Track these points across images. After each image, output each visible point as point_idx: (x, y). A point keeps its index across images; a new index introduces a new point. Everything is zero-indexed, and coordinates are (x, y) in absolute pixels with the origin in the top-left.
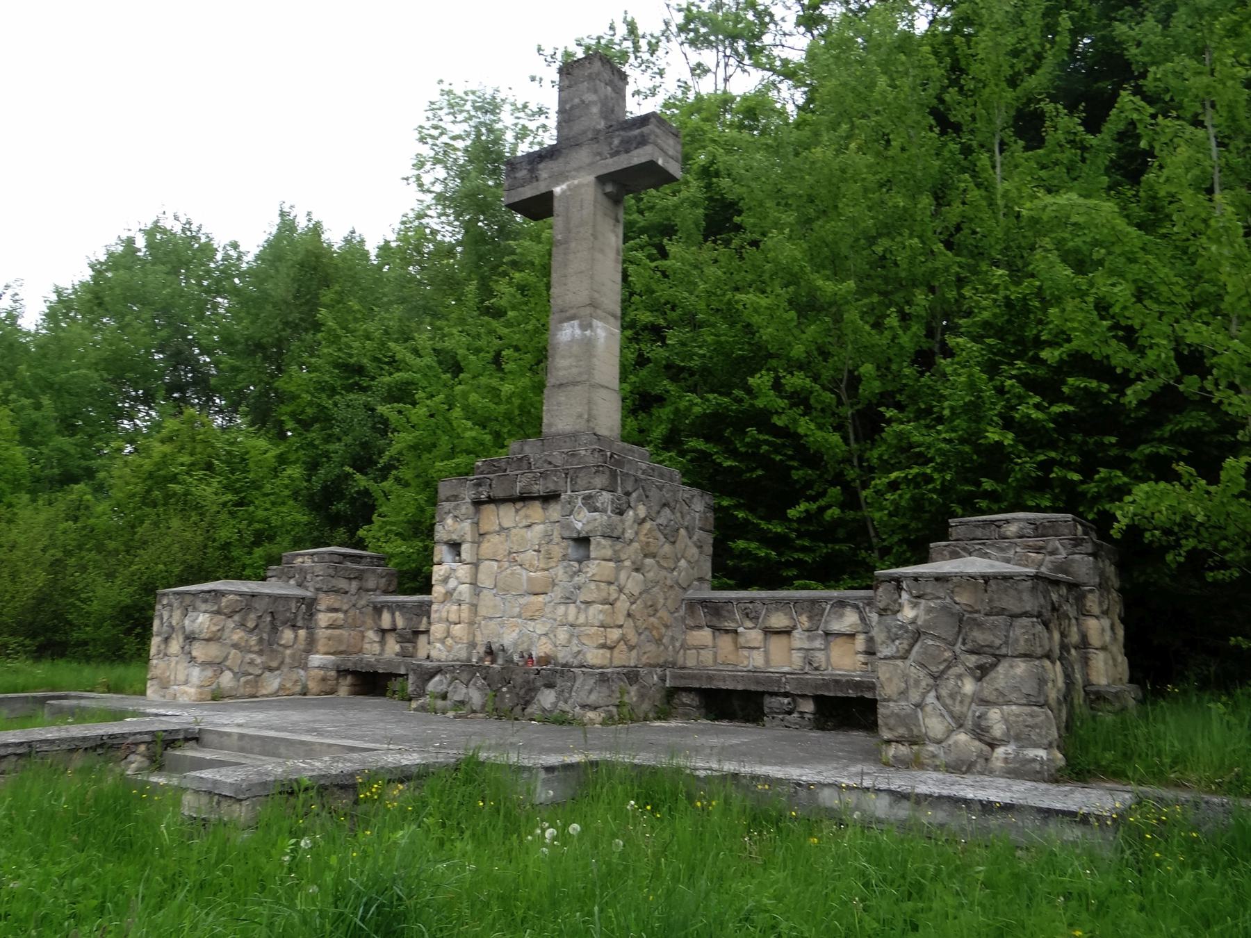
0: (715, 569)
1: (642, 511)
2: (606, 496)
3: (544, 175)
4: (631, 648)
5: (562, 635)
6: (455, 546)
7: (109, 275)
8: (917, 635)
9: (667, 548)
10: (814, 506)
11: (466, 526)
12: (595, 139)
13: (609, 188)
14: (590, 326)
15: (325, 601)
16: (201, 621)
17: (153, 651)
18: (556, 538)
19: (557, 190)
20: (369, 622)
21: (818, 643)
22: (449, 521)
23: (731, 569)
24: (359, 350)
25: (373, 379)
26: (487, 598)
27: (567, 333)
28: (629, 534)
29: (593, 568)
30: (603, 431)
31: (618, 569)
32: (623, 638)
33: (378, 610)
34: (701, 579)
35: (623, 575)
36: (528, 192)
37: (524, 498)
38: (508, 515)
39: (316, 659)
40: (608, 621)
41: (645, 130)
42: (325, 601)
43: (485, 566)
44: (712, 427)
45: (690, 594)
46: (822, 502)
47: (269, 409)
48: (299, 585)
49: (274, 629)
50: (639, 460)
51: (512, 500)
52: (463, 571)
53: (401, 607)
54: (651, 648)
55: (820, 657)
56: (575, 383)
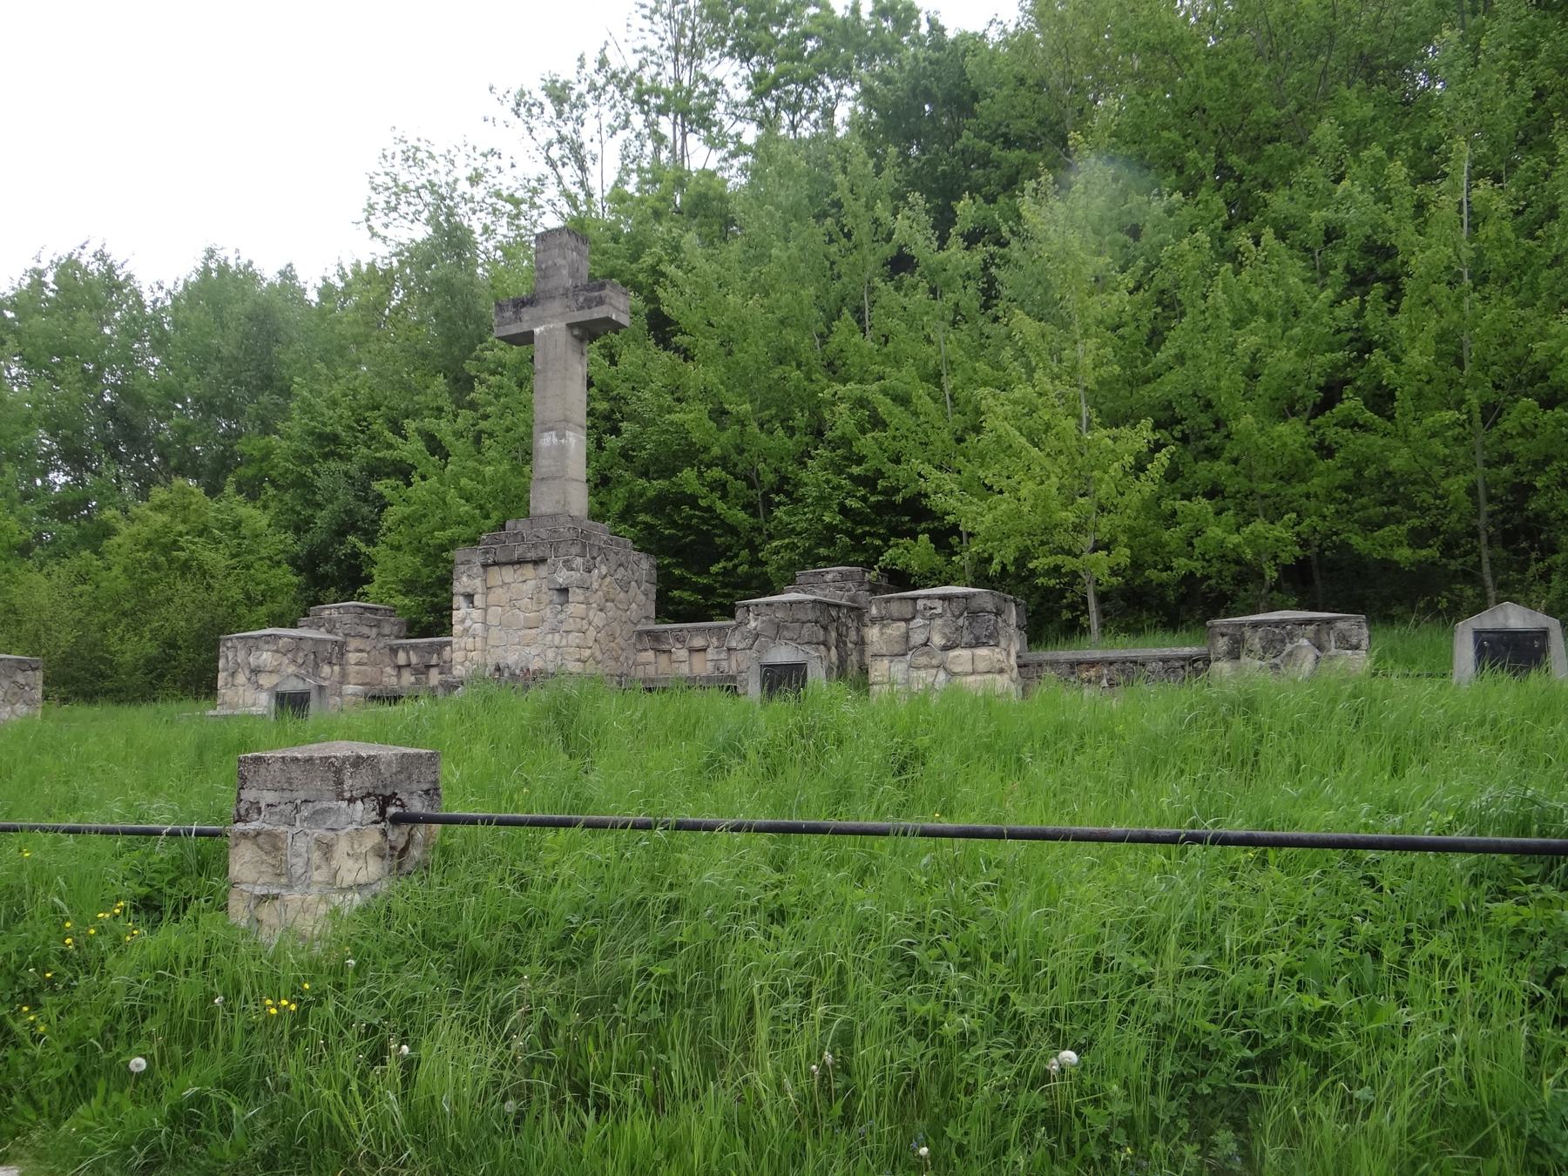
0: (658, 612)
1: (604, 570)
2: (579, 560)
3: (526, 317)
4: (598, 663)
5: (550, 654)
6: (469, 597)
7: (9, 315)
8: (757, 636)
9: (622, 595)
10: (730, 565)
11: (478, 582)
12: (565, 295)
13: (576, 332)
14: (564, 436)
15: (354, 643)
16: (266, 657)
17: (220, 683)
18: (544, 589)
19: (537, 331)
20: (387, 660)
21: (723, 656)
22: (465, 579)
23: (667, 609)
24: (335, 420)
25: (350, 447)
26: (494, 632)
27: (546, 441)
28: (595, 586)
29: (570, 608)
30: (574, 513)
31: (588, 609)
32: (592, 655)
33: (394, 651)
34: (647, 618)
35: (591, 613)
36: (514, 329)
37: (521, 562)
38: (508, 574)
39: (350, 689)
40: (582, 643)
41: (603, 293)
42: (354, 643)
43: (491, 610)
44: (658, 504)
45: (639, 627)
46: (736, 561)
47: (222, 471)
48: (329, 632)
49: (316, 666)
50: (601, 531)
51: (512, 563)
52: (476, 614)
53: (414, 647)
54: (613, 663)
55: (724, 664)
56: (554, 478)
